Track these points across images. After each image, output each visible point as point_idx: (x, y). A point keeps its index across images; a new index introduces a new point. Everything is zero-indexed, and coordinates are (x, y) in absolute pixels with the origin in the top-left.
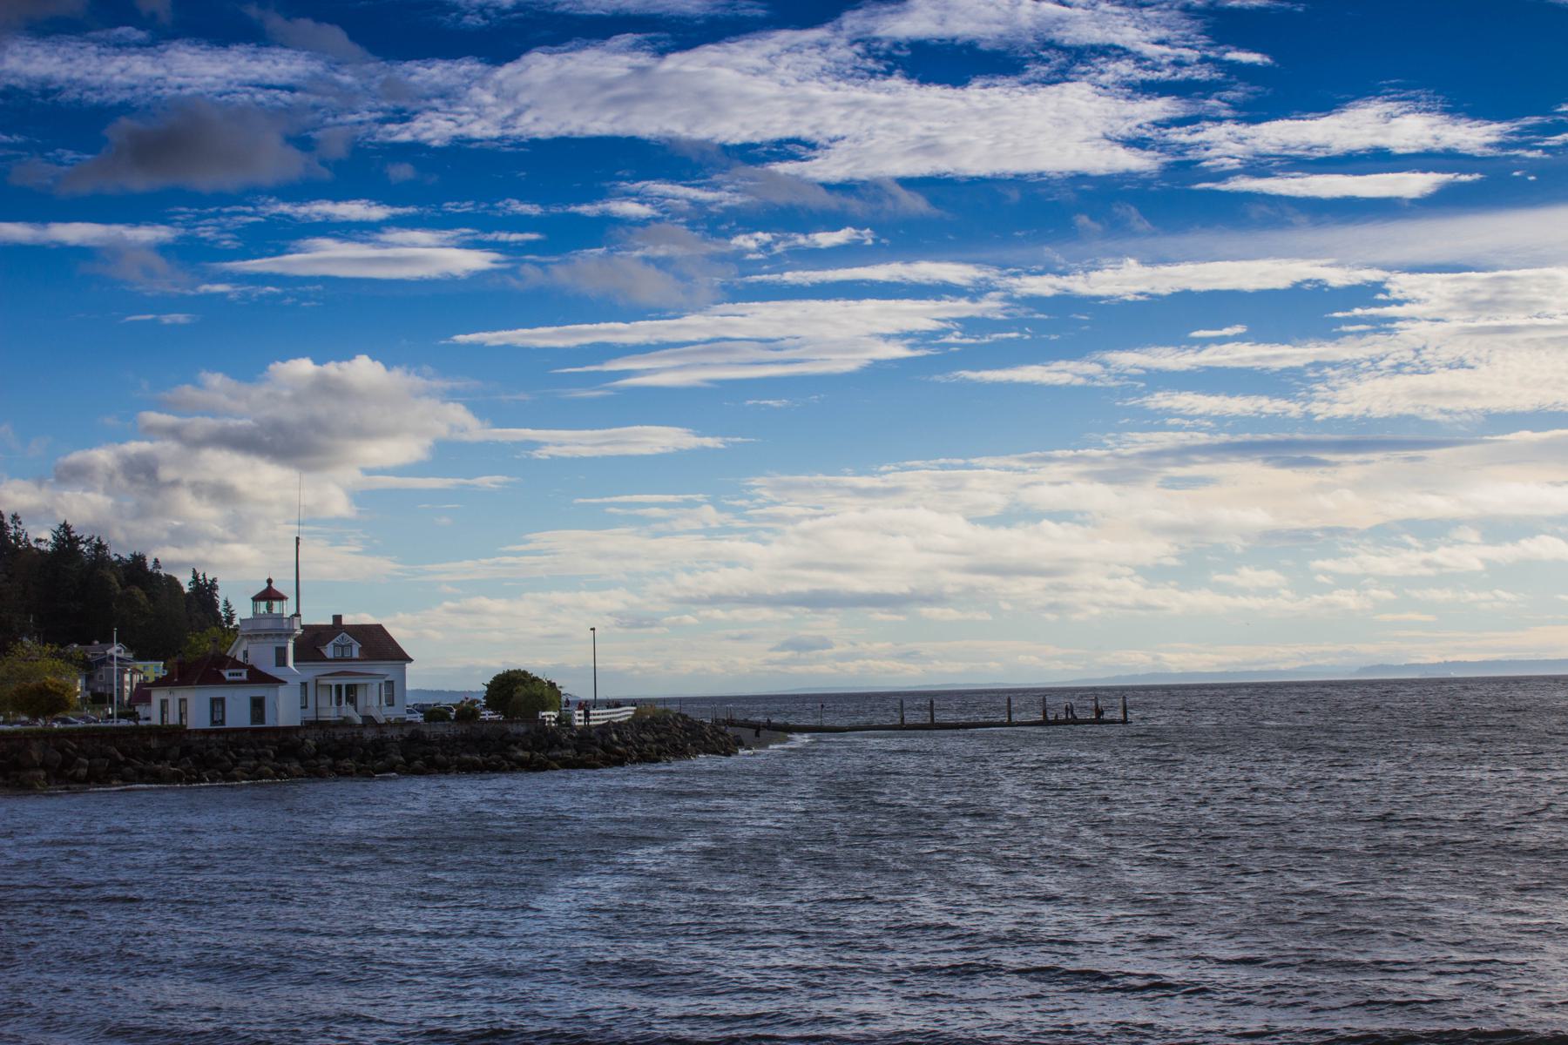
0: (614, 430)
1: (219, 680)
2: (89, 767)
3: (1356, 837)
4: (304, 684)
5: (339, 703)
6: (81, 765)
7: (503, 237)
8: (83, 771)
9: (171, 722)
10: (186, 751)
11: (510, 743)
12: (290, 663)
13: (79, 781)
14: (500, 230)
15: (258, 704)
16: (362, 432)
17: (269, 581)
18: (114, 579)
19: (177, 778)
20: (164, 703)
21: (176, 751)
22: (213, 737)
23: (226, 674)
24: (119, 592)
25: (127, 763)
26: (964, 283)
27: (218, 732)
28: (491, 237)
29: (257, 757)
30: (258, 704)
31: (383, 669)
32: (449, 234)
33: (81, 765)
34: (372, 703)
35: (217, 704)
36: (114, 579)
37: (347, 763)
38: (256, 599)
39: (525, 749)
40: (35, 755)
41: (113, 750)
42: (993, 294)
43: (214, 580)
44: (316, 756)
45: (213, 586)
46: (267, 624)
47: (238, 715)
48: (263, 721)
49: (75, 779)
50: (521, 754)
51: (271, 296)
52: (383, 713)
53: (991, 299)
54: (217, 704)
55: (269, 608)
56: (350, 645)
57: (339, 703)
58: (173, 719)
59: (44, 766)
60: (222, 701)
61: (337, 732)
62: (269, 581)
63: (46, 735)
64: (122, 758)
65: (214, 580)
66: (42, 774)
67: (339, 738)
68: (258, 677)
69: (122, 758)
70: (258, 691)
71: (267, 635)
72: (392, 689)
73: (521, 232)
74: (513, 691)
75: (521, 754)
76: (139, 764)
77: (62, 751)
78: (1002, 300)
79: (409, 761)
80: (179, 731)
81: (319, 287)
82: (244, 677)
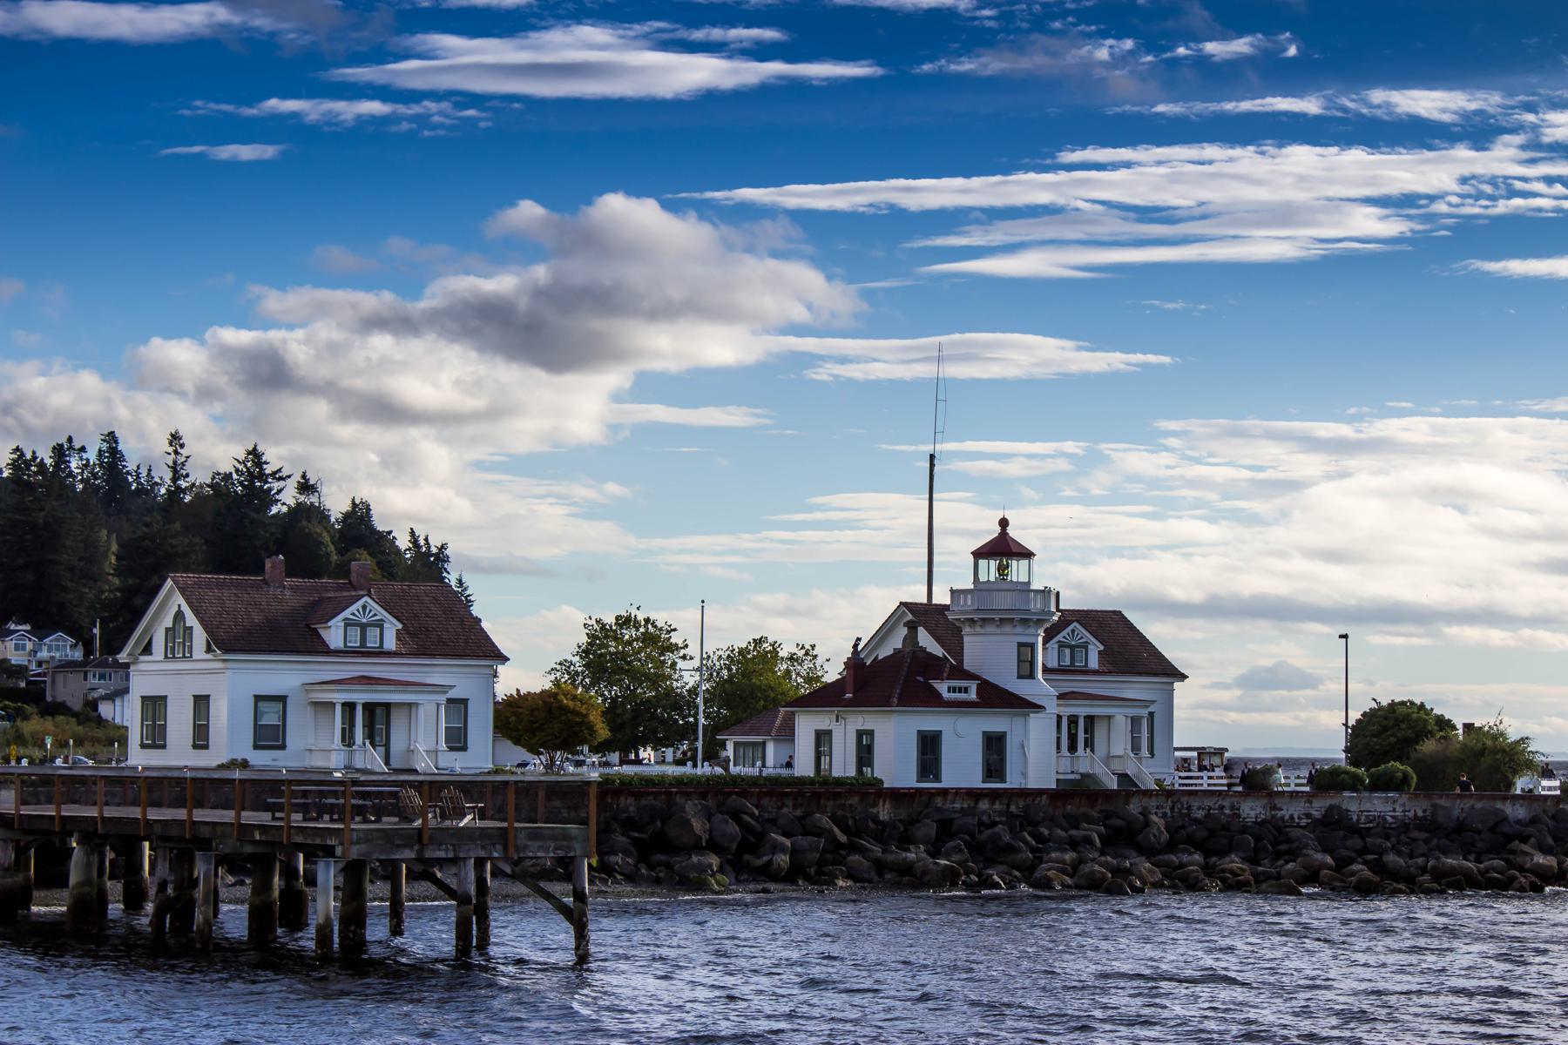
0: (969, 336)
1: (933, 700)
2: (794, 852)
3: (957, 1006)
4: (1059, 717)
5: (1073, 748)
6: (776, 848)
7: (717, 34)
8: (783, 860)
9: (837, 772)
10: (946, 828)
11: (1510, 838)
12: (1040, 675)
13: (775, 878)
14: (714, 25)
15: (994, 745)
16: (663, 312)
17: (1004, 523)
18: (327, 539)
19: (949, 878)
20: (822, 738)
21: (929, 829)
22: (984, 805)
23: (942, 687)
24: (334, 558)
25: (853, 848)
26: (1446, 118)
27: (994, 795)
28: (698, 35)
29: (1074, 844)
30: (994, 745)
31: (1136, 688)
32: (638, 28)
33: (776, 848)
34: (1111, 758)
35: (929, 745)
36: (327, 539)
37: (1235, 862)
38: (978, 554)
39: (1546, 851)
40: (697, 825)
41: (824, 821)
42: (1507, 138)
43: (443, 547)
44: (1171, 847)
45: (441, 557)
46: (1004, 601)
47: (962, 768)
48: (937, 779)
49: (768, 874)
50: (1540, 859)
51: (374, 120)
52: (1148, 773)
53: (1507, 145)
54: (929, 745)
55: (1002, 569)
56: (1085, 646)
57: (1073, 748)
58: (843, 765)
59: (713, 846)
60: (871, 733)
61: (1195, 804)
62: (1004, 523)
63: (721, 791)
64: (843, 838)
65: (443, 547)
66: (714, 861)
67: (1200, 814)
68: (994, 697)
69: (843, 838)
70: (995, 722)
71: (1005, 621)
72: (1152, 726)
73: (747, 26)
74: (1393, 737)
75: (1540, 859)
76: (876, 850)
77: (736, 816)
78: (1523, 147)
79: (1341, 864)
80: (866, 789)
81: (445, 105)
82: (973, 695)
